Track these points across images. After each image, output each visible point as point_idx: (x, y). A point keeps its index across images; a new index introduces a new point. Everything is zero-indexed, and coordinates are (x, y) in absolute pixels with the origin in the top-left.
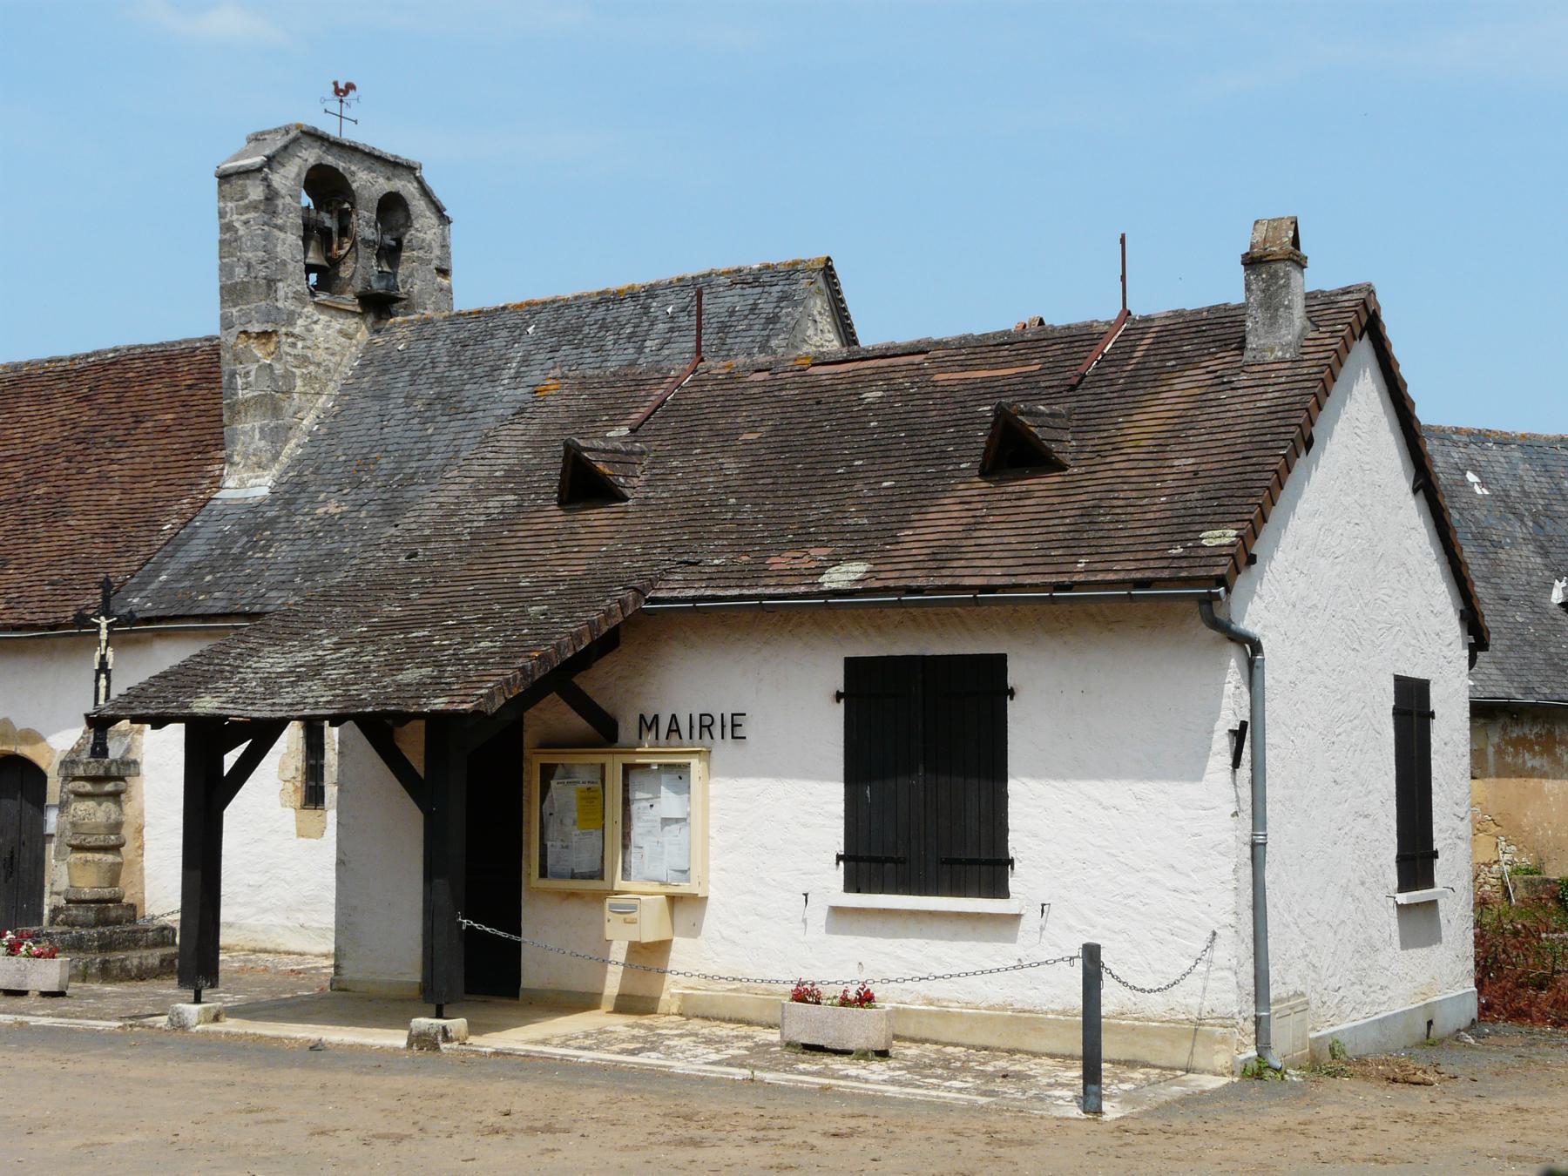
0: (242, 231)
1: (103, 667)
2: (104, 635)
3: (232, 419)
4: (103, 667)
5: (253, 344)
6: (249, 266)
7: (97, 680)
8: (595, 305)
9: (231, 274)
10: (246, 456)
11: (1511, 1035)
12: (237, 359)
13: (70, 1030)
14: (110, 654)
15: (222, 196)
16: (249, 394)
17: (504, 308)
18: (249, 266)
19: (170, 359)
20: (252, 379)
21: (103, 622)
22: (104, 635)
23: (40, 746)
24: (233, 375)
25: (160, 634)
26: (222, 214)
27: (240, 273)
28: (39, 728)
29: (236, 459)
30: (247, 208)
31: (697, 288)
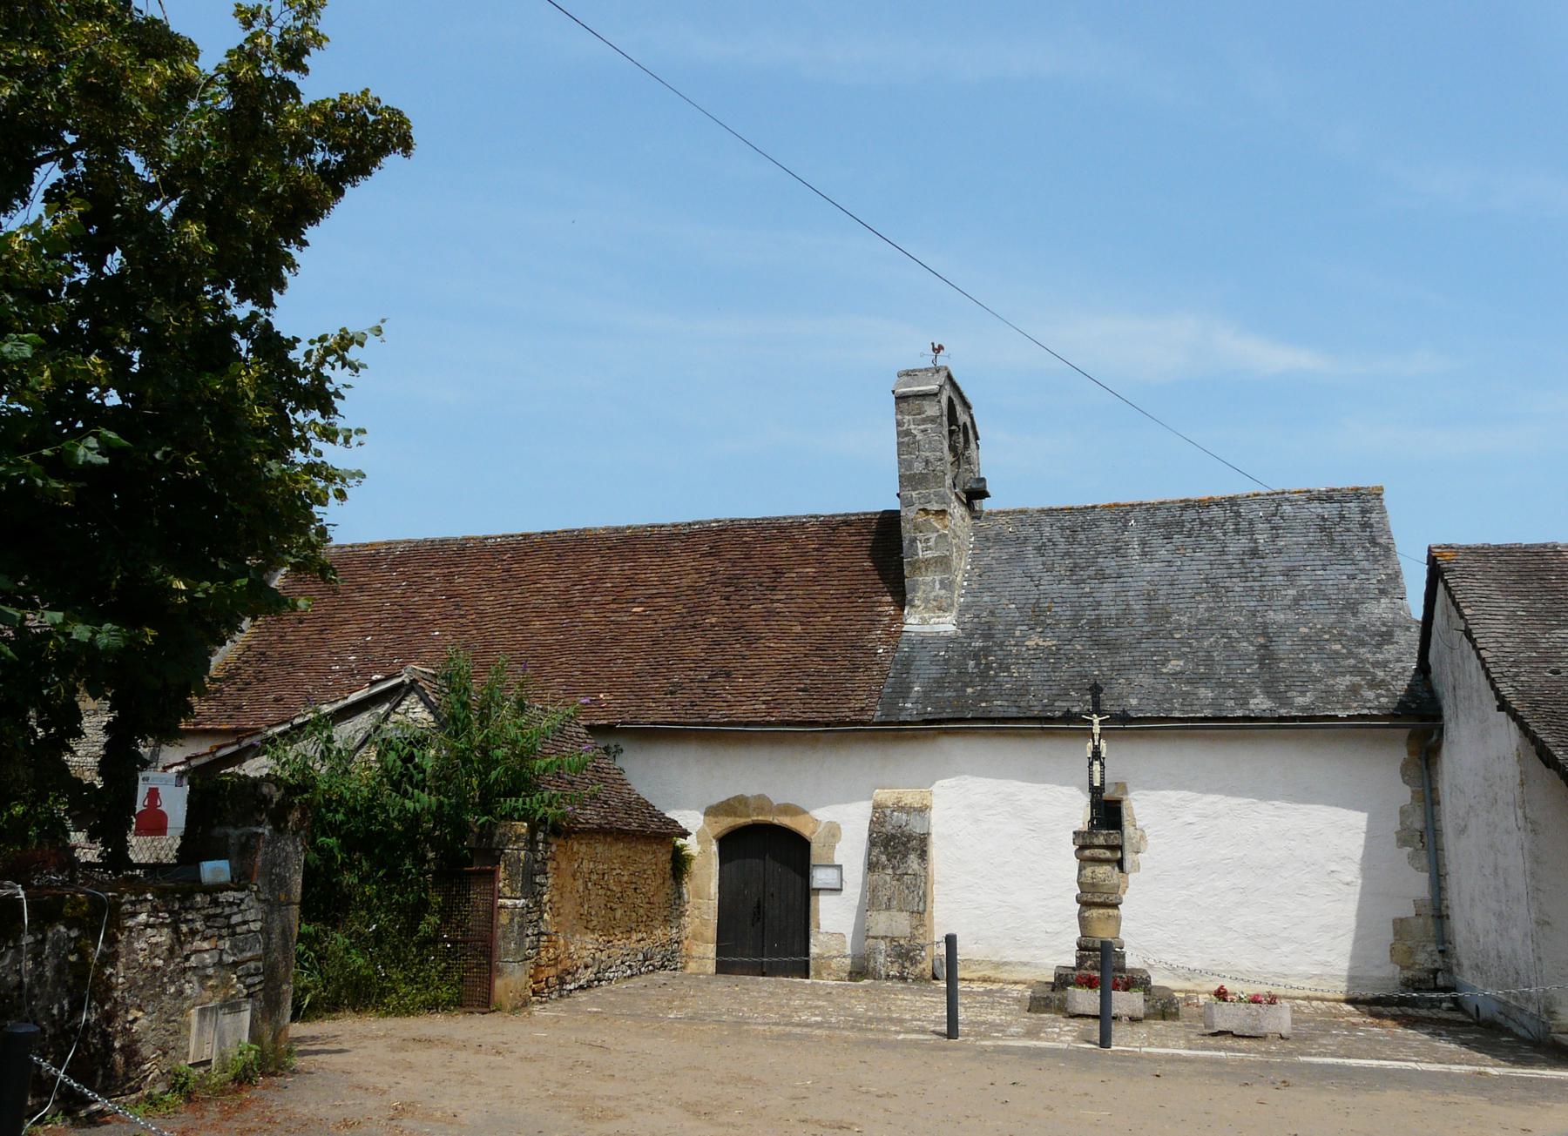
0: (919, 437)
1: (1096, 754)
2: (1097, 729)
3: (913, 573)
4: (1096, 754)
5: (932, 518)
6: (927, 462)
7: (1091, 764)
8: (1183, 509)
9: (910, 465)
10: (926, 601)
11: (722, 977)
12: (917, 528)
13: (1531, 1079)
14: (1103, 744)
15: (899, 411)
16: (929, 555)
17: (1094, 507)
18: (927, 462)
19: (781, 529)
20: (931, 543)
21: (1096, 720)
22: (1097, 729)
23: (801, 818)
24: (914, 540)
25: (947, 732)
26: (899, 424)
27: (918, 467)
28: (800, 804)
29: (917, 602)
30: (924, 421)
31: (1277, 499)
